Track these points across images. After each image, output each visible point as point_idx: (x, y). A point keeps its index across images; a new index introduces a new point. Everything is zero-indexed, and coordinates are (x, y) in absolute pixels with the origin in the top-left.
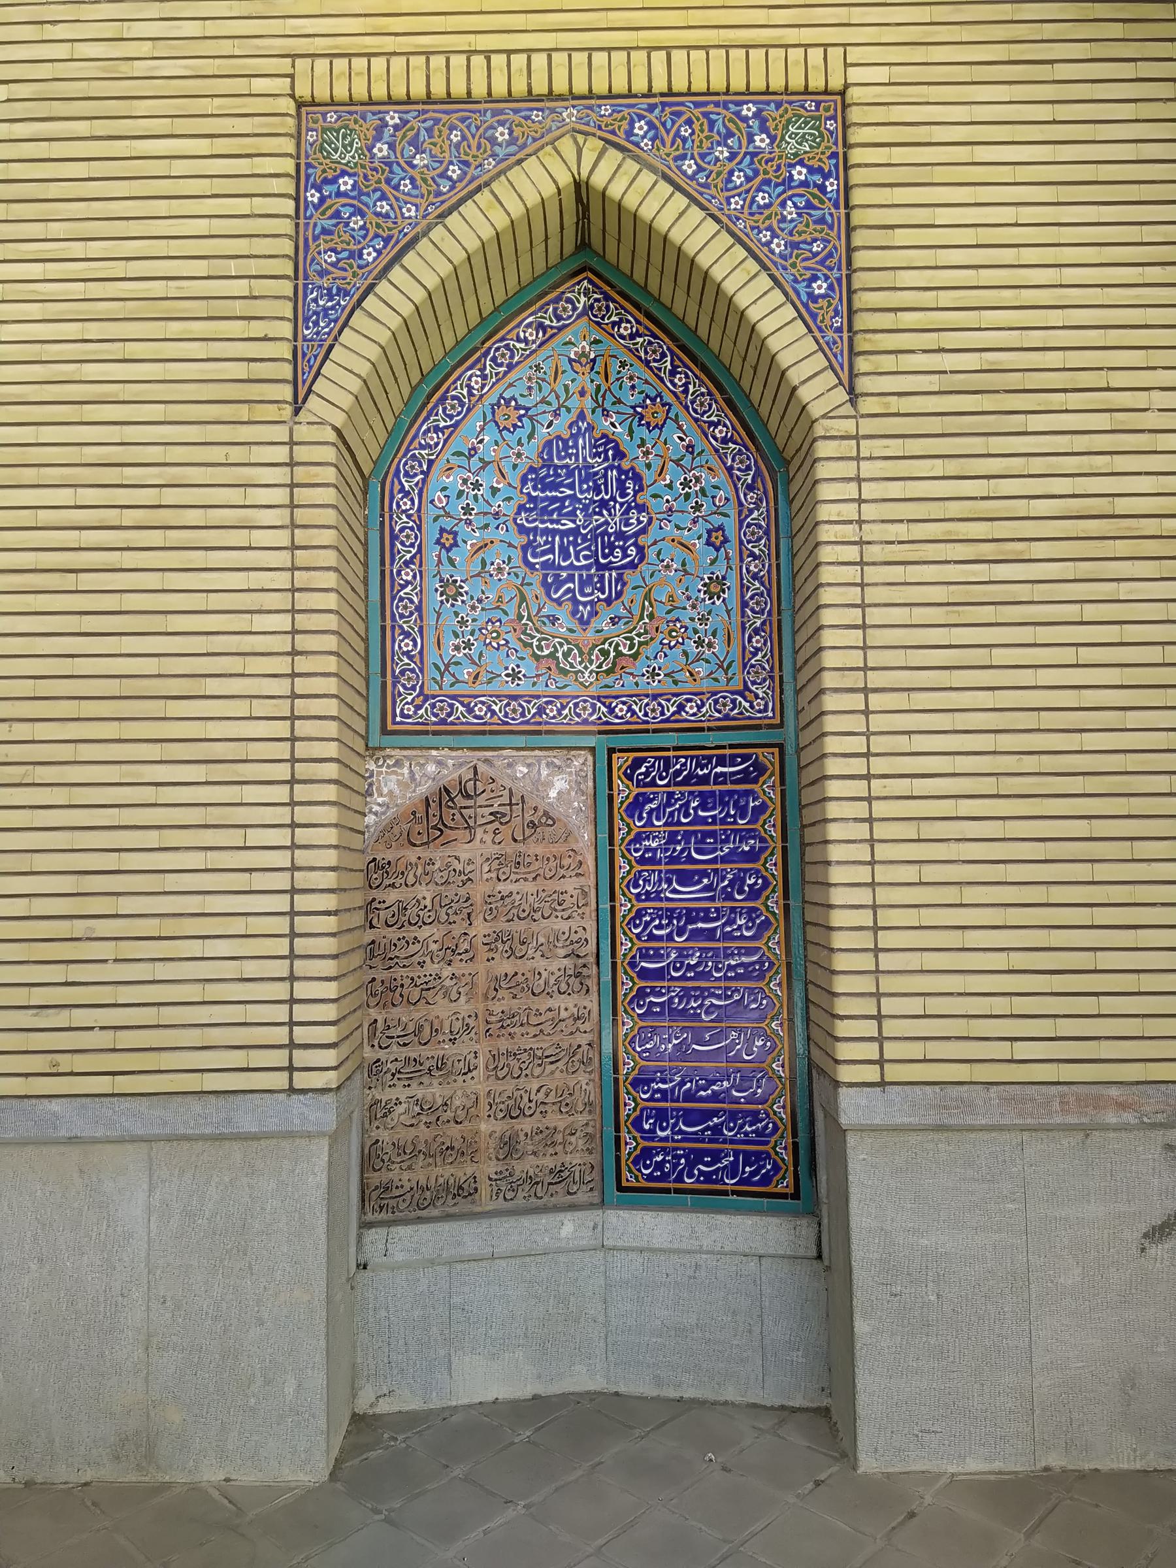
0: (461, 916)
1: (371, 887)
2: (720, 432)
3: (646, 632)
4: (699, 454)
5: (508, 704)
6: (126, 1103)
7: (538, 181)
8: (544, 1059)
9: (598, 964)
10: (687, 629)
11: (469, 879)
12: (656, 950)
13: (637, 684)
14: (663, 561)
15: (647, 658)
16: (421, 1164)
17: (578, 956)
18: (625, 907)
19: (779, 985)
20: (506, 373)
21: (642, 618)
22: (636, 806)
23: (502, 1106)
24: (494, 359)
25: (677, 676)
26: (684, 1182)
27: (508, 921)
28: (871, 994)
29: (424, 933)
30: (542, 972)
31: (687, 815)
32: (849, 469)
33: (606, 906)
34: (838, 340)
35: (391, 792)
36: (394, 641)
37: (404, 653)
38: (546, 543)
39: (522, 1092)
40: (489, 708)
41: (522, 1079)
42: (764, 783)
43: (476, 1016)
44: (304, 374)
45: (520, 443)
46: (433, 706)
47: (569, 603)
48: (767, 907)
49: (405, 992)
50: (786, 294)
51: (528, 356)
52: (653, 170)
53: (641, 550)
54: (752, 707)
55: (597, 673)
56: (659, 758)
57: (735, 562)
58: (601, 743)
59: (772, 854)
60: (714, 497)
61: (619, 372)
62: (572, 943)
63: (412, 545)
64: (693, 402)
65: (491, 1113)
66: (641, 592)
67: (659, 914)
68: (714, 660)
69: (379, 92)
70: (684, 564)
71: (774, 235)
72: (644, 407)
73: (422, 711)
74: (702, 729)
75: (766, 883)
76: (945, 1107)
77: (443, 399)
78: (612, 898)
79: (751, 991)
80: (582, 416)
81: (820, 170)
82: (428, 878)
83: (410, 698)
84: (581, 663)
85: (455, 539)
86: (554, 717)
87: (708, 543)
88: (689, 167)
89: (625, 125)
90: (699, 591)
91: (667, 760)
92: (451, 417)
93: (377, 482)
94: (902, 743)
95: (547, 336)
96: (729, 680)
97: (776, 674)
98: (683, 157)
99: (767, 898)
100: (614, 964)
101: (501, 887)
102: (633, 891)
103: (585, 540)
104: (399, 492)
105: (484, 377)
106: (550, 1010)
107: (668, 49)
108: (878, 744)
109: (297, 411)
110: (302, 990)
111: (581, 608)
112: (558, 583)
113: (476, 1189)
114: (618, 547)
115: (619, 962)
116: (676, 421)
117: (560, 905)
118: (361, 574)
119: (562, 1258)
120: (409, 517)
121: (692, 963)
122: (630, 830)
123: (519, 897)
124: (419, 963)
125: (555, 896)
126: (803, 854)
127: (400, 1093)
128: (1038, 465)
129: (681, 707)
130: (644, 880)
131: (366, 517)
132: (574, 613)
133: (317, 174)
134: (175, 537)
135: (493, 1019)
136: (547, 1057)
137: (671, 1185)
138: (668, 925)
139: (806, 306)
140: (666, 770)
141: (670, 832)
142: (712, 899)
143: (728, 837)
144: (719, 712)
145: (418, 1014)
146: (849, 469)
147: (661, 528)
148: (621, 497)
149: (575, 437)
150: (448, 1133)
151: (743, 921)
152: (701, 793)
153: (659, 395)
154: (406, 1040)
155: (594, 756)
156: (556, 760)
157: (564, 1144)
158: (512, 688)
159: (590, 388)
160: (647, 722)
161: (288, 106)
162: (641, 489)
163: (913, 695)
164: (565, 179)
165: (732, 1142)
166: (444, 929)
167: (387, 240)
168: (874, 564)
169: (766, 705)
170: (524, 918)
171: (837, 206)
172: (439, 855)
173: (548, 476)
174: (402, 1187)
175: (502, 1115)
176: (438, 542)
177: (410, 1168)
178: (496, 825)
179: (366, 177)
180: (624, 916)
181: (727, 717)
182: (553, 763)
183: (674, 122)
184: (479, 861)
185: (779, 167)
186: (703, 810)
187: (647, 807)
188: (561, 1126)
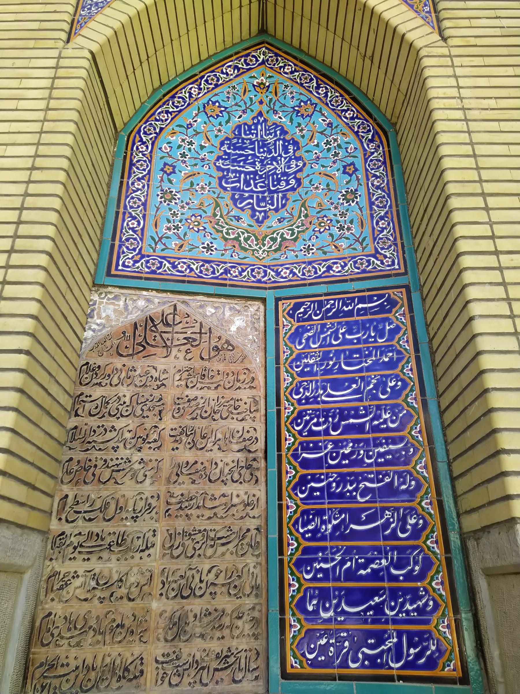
0: (154, 412)
1: (81, 383)
3: (303, 225)
4: (336, 127)
5: (203, 265)
8: (216, 541)
10: (331, 220)
11: (163, 385)
12: (316, 443)
13: (297, 256)
14: (314, 185)
15: (304, 240)
16: (90, 641)
17: (249, 451)
18: (288, 410)
19: (425, 467)
20: (213, 89)
21: (300, 217)
22: (296, 336)
23: (174, 585)
24: (207, 81)
25: (325, 249)
26: (348, 667)
27: (193, 419)
30: (219, 462)
31: (337, 339)
33: (272, 410)
35: (108, 317)
36: (124, 220)
37: (130, 229)
38: (235, 177)
39: (194, 572)
41: (195, 559)
42: (396, 312)
43: (158, 497)
44: (76, 30)
45: (220, 124)
46: (147, 262)
47: (250, 211)
48: (407, 403)
49: (97, 472)
51: (227, 81)
53: (299, 182)
54: (382, 263)
55: (268, 252)
56: (314, 302)
57: (363, 181)
58: (270, 295)
60: (346, 148)
61: (284, 91)
62: (244, 440)
65: (164, 591)
66: (299, 203)
67: (316, 413)
70: (328, 185)
72: (300, 106)
73: (137, 265)
77: (173, 97)
79: (400, 474)
80: (260, 114)
82: (129, 381)
83: (130, 256)
84: (256, 245)
85: (174, 169)
86: (236, 276)
87: (344, 172)
90: (339, 199)
95: (240, 72)
96: (363, 249)
97: (399, 241)
100: (280, 457)
101: (188, 392)
102: (295, 397)
104: (139, 141)
106: (224, 495)
111: (257, 213)
112: (242, 199)
113: (142, 672)
114: (284, 180)
116: (320, 112)
118: (107, 181)
121: (346, 452)
123: (202, 401)
124: (113, 448)
125: (232, 402)
129: (329, 268)
130: (304, 389)
132: (253, 216)
135: (173, 500)
136: (219, 539)
137: (336, 671)
138: (324, 423)
140: (320, 308)
141: (324, 352)
142: (360, 400)
148: (285, 154)
149: (256, 125)
150: (121, 610)
151: (388, 416)
152: (347, 323)
153: (310, 100)
154: (92, 515)
155: (265, 306)
156: (236, 306)
157: (231, 627)
158: (207, 256)
159: (266, 100)
160: (305, 279)
162: (298, 148)
165: (395, 621)
166: (137, 421)
170: (206, 418)
172: (140, 364)
173: (238, 143)
174: (68, 665)
175: (173, 594)
176: (162, 170)
177: (78, 644)
178: (188, 346)
180: (288, 417)
182: (234, 308)
186: (349, 335)
187: (305, 335)
188: (229, 609)
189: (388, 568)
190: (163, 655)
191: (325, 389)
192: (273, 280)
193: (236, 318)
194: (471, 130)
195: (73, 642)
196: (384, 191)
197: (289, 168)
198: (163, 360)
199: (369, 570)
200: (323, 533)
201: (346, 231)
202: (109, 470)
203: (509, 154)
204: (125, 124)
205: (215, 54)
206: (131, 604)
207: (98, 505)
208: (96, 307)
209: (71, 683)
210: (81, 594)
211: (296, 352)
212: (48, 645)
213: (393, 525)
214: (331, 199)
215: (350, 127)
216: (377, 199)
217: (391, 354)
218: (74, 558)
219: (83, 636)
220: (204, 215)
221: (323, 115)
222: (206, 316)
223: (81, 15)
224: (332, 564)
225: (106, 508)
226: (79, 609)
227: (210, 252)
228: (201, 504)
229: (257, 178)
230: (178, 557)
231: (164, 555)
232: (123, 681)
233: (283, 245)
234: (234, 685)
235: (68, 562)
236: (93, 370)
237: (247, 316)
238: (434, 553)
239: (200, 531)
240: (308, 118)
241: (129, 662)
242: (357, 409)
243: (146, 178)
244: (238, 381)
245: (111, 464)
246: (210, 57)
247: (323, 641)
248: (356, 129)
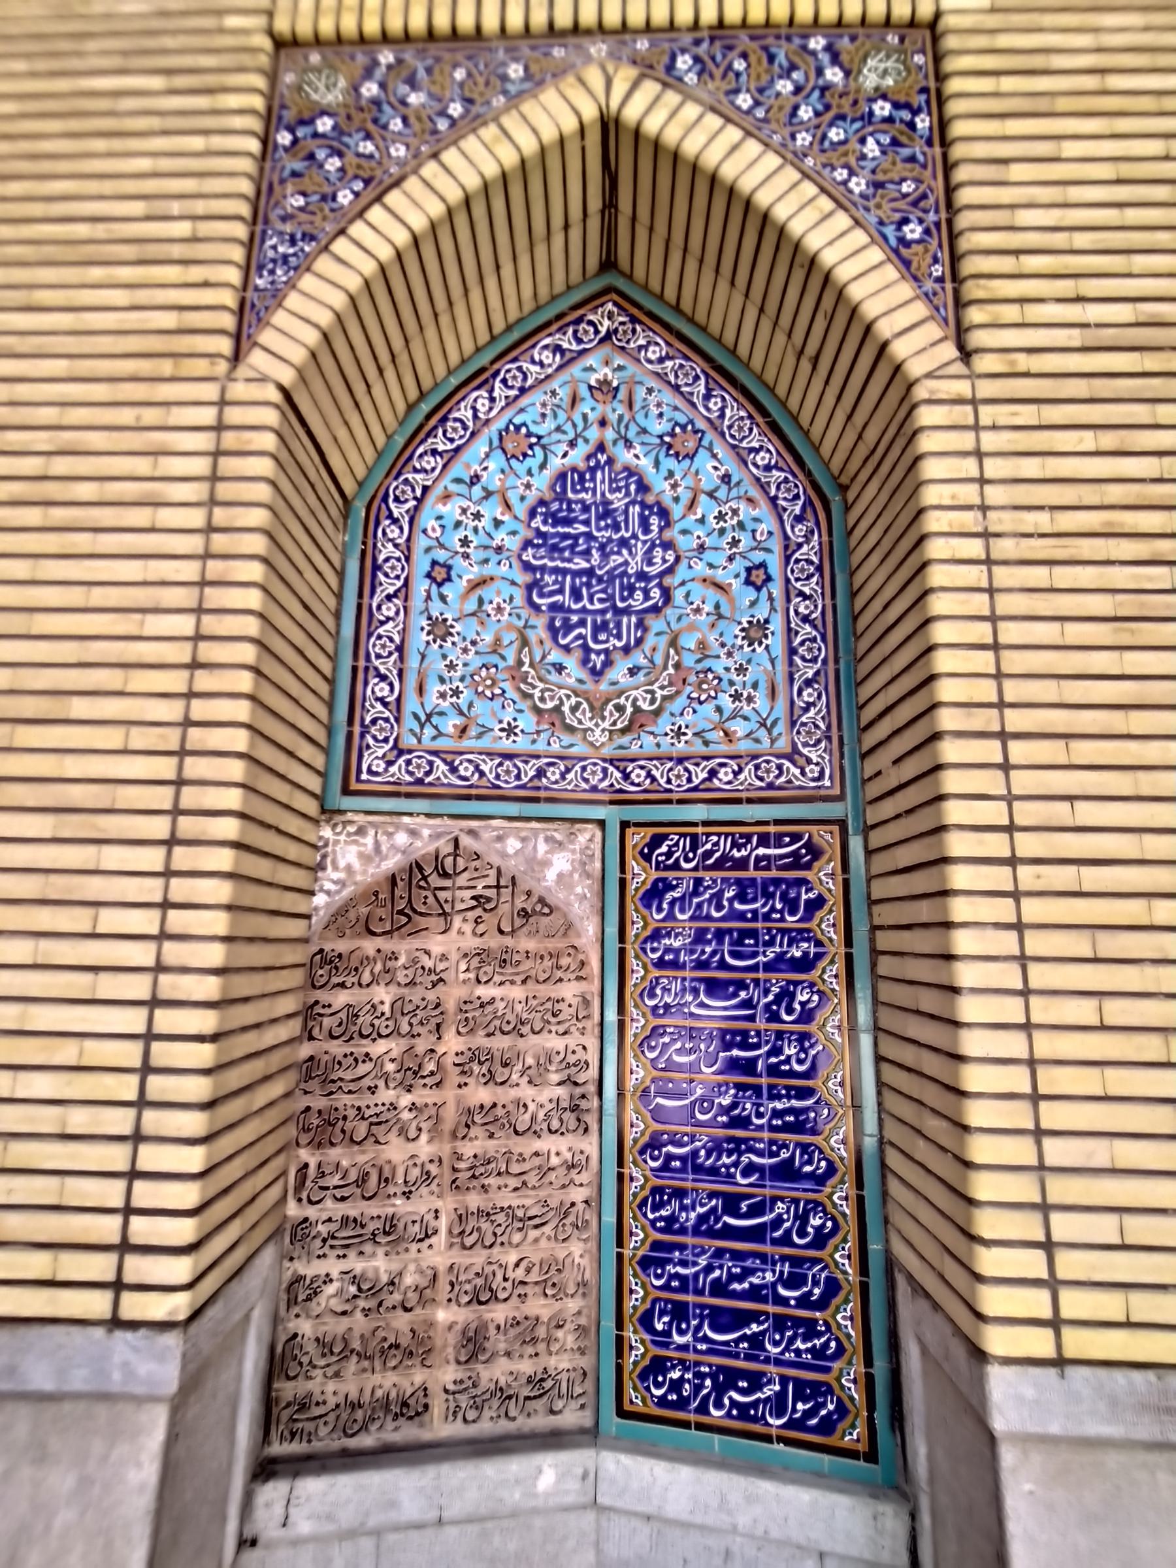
0: (429, 1027)
2: (762, 459)
3: (671, 684)
4: (738, 484)
5: (500, 764)
7: (555, 113)
8: (526, 1221)
10: (720, 680)
11: (441, 980)
13: (658, 745)
15: (672, 714)
17: (576, 1084)
21: (665, 668)
22: (654, 894)
23: (468, 1287)
25: (709, 736)
26: (708, 1413)
27: (488, 1035)
28: (1032, 1206)
29: (379, 1048)
34: (939, 290)
36: (366, 683)
37: (377, 699)
38: (555, 582)
39: (495, 1267)
40: (477, 767)
41: (496, 1249)
43: (440, 1161)
46: (408, 762)
49: (349, 1126)
53: (667, 594)
54: (803, 773)
55: (611, 732)
57: (779, 604)
60: (754, 531)
62: (568, 1066)
71: (852, 173)
72: (672, 434)
77: (444, 419)
79: (804, 1148)
80: (601, 448)
81: (907, 106)
82: (388, 977)
83: (380, 753)
84: (591, 719)
87: (748, 582)
89: (666, 59)
90: (736, 637)
91: (694, 838)
98: (737, 91)
105: (492, 400)
106: (537, 1154)
108: (1026, 813)
110: (151, 1157)
111: (593, 656)
112: (568, 627)
113: (426, 1406)
116: (710, 449)
117: (554, 1015)
119: (538, 1522)
123: (503, 1005)
124: (369, 1088)
126: (874, 965)
127: (334, 1267)
129: (713, 773)
130: (664, 989)
132: (585, 661)
133: (289, 116)
134: (59, 515)
135: (462, 1165)
136: (530, 1218)
137: (692, 1417)
140: (694, 848)
142: (751, 1018)
143: (773, 938)
144: (761, 779)
147: (690, 567)
151: (793, 1051)
152: (739, 882)
153: (691, 422)
154: (345, 1192)
155: (603, 830)
157: (549, 1340)
158: (506, 745)
160: (670, 791)
162: (668, 524)
164: (590, 112)
165: (778, 1362)
166: (404, 1044)
167: (367, 182)
169: (822, 772)
171: (929, 143)
172: (404, 947)
173: (560, 510)
174: (324, 1403)
175: (466, 1299)
176: (429, 575)
177: (337, 1375)
178: (479, 912)
179: (349, 117)
183: (724, 56)
184: (454, 956)
185: (855, 102)
187: (669, 896)
188: (545, 1314)
189: (774, 1285)
190: (455, 1382)
191: (695, 991)
192: (618, 786)
193: (556, 856)
194: (996, 585)
195: (330, 1371)
196: (815, 627)
197: (650, 563)
198: (440, 937)
199: (746, 1285)
200: (682, 1224)
201: (744, 703)
202: (365, 1124)
203: (1060, 642)
204: (360, 484)
205: (520, 321)
206: (407, 1315)
207: (353, 1176)
208: (329, 849)
209: (331, 1427)
210: (337, 1305)
211: (653, 925)
212: (295, 1377)
213: (787, 1225)
214: (721, 635)
215: (762, 487)
216: (802, 643)
217: (806, 945)
218: (324, 1255)
219: (344, 1363)
220: (502, 665)
221: (714, 456)
222: (507, 855)
223: (256, 289)
224: (693, 1270)
225: (364, 1181)
226: (335, 1327)
227: (513, 738)
228: (503, 1169)
229: (594, 582)
230: (471, 1247)
231: (452, 1245)
232: (402, 1420)
233: (637, 722)
234: (552, 1417)
235: (316, 1262)
236: (331, 962)
237: (573, 852)
238: (845, 1273)
239: (502, 1209)
240: (688, 461)
241: (408, 1394)
242: (745, 1034)
243: (402, 595)
244: (559, 968)
245: (368, 1113)
246: (509, 328)
248: (773, 493)
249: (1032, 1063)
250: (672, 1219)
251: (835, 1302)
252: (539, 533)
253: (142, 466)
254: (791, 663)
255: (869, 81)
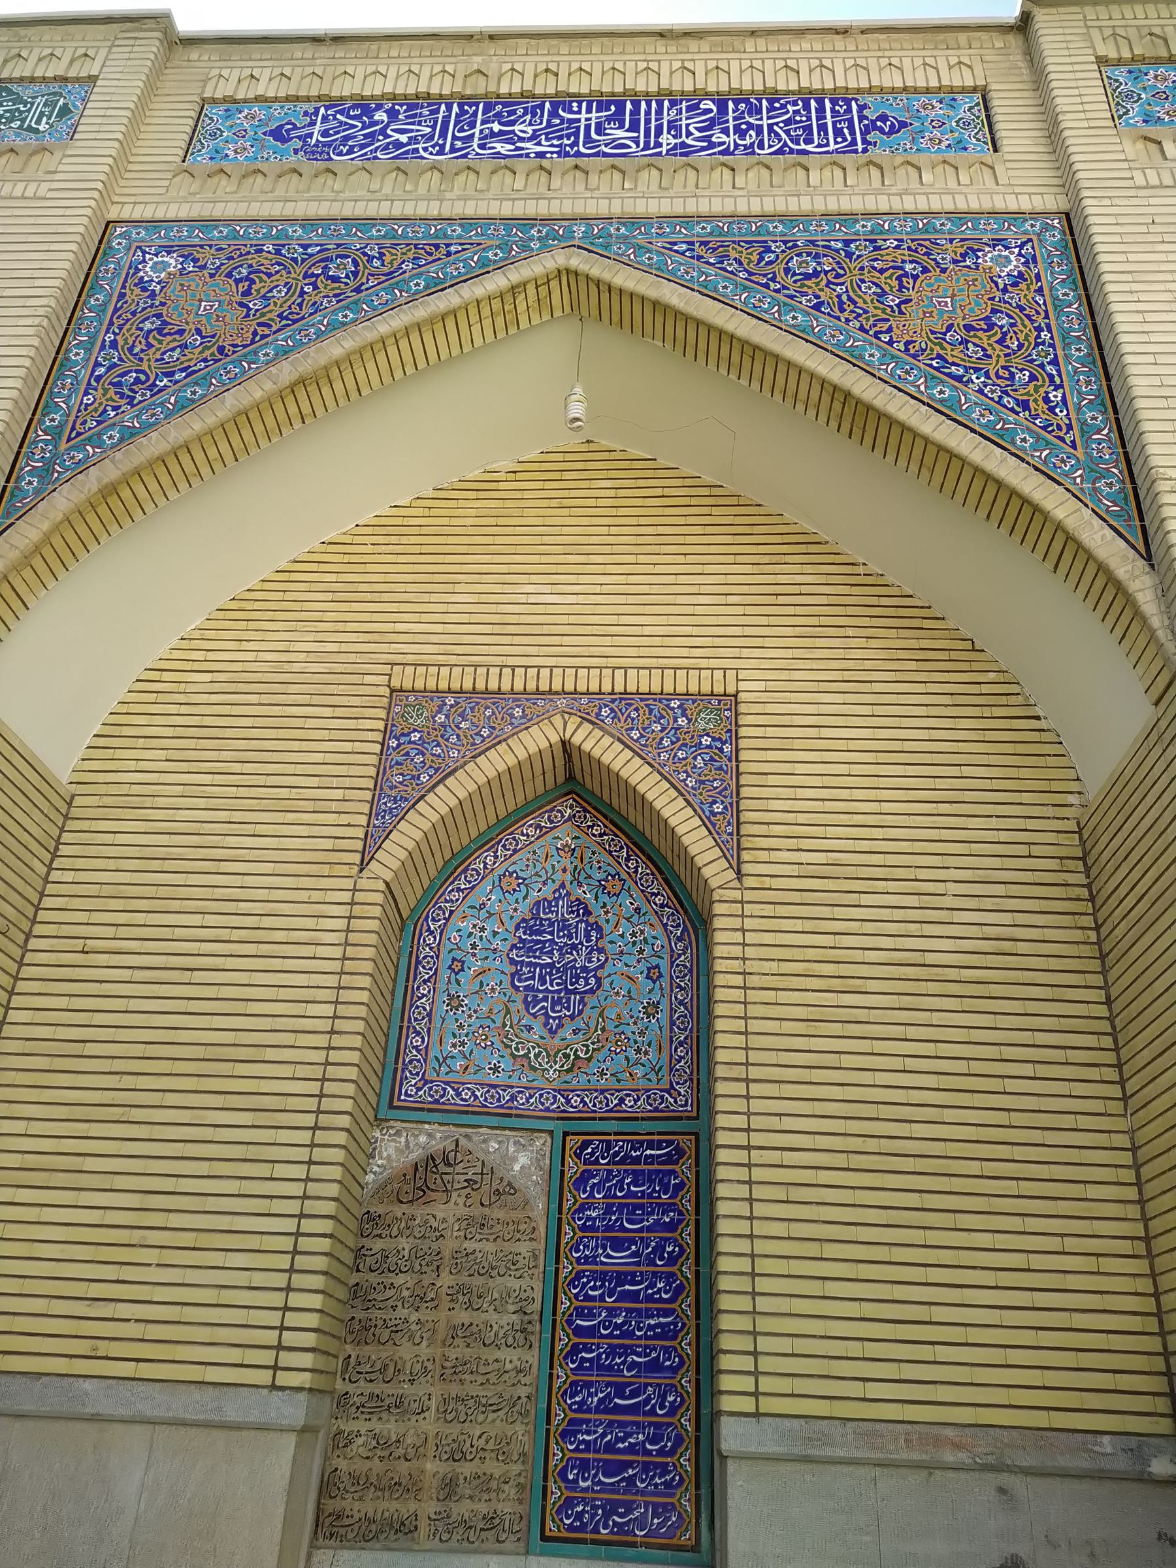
3: (599, 1041)
5: (488, 1091)
6: (141, 1387)
7: (538, 739)
9: (541, 1322)
11: (442, 1236)
12: (590, 1309)
13: (589, 1081)
17: (525, 1313)
18: (567, 1269)
20: (511, 855)
21: (596, 1031)
22: (581, 1181)
23: (447, 1449)
26: (599, 1532)
28: (749, 1333)
29: (400, 1280)
32: (736, 923)
35: (389, 1156)
38: (529, 972)
41: (467, 1424)
45: (517, 901)
46: (430, 1089)
49: (377, 1332)
50: (695, 810)
52: (612, 736)
53: (599, 981)
54: (676, 1102)
57: (667, 991)
58: (558, 1127)
59: (687, 1225)
62: (521, 1301)
63: (431, 969)
64: (641, 879)
66: (597, 1011)
67: (594, 1276)
68: (648, 1064)
69: (443, 686)
72: (607, 881)
74: (636, 1119)
75: (682, 1251)
76: (810, 1439)
77: (466, 870)
78: (557, 1261)
79: (666, 1349)
80: (563, 886)
81: (720, 739)
83: (413, 1082)
87: (648, 977)
88: (635, 734)
91: (608, 1142)
92: (470, 882)
93: (410, 925)
94: (774, 1122)
97: (695, 1077)
98: (632, 729)
99: (682, 1265)
100: (554, 1321)
101: (466, 1244)
103: (558, 971)
105: (496, 857)
106: (497, 1361)
107: (626, 669)
108: (757, 1122)
109: (361, 870)
112: (536, 1002)
113: (416, 1527)
115: (558, 1319)
116: (629, 891)
117: (514, 1265)
120: (431, 949)
121: (619, 1322)
122: (576, 1201)
127: (362, 1426)
128: (869, 928)
129: (622, 1101)
131: (400, 947)
132: (546, 1024)
133: (398, 731)
134: (265, 949)
135: (448, 1364)
137: (588, 1536)
138: (601, 1287)
139: (708, 818)
140: (608, 1150)
141: (607, 1204)
142: (638, 1264)
144: (651, 1105)
145: (385, 1353)
146: (736, 923)
153: (618, 873)
157: (498, 1491)
159: (570, 867)
160: (595, 1112)
161: (387, 692)
162: (602, 937)
163: (783, 1086)
164: (555, 738)
167: (437, 770)
168: (754, 988)
169: (687, 1101)
171: (730, 760)
172: (420, 1212)
173: (535, 925)
176: (450, 967)
177: (361, 1499)
179: (428, 733)
181: (656, 1110)
185: (693, 737)
189: (644, 1442)
195: (357, 1496)
207: (378, 1366)
211: (580, 1201)
220: (492, 1026)
221: (631, 896)
226: (360, 1466)
235: (351, 1421)
238: (686, 1430)
242: (633, 1274)
247: (580, 1509)
249: (753, 1256)
250: (583, 1402)
251: (680, 1451)
252: (521, 940)
253: (310, 923)
254: (671, 1029)
255: (701, 725)
